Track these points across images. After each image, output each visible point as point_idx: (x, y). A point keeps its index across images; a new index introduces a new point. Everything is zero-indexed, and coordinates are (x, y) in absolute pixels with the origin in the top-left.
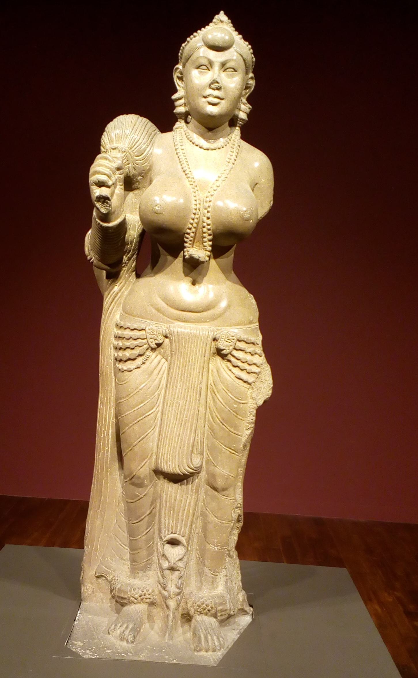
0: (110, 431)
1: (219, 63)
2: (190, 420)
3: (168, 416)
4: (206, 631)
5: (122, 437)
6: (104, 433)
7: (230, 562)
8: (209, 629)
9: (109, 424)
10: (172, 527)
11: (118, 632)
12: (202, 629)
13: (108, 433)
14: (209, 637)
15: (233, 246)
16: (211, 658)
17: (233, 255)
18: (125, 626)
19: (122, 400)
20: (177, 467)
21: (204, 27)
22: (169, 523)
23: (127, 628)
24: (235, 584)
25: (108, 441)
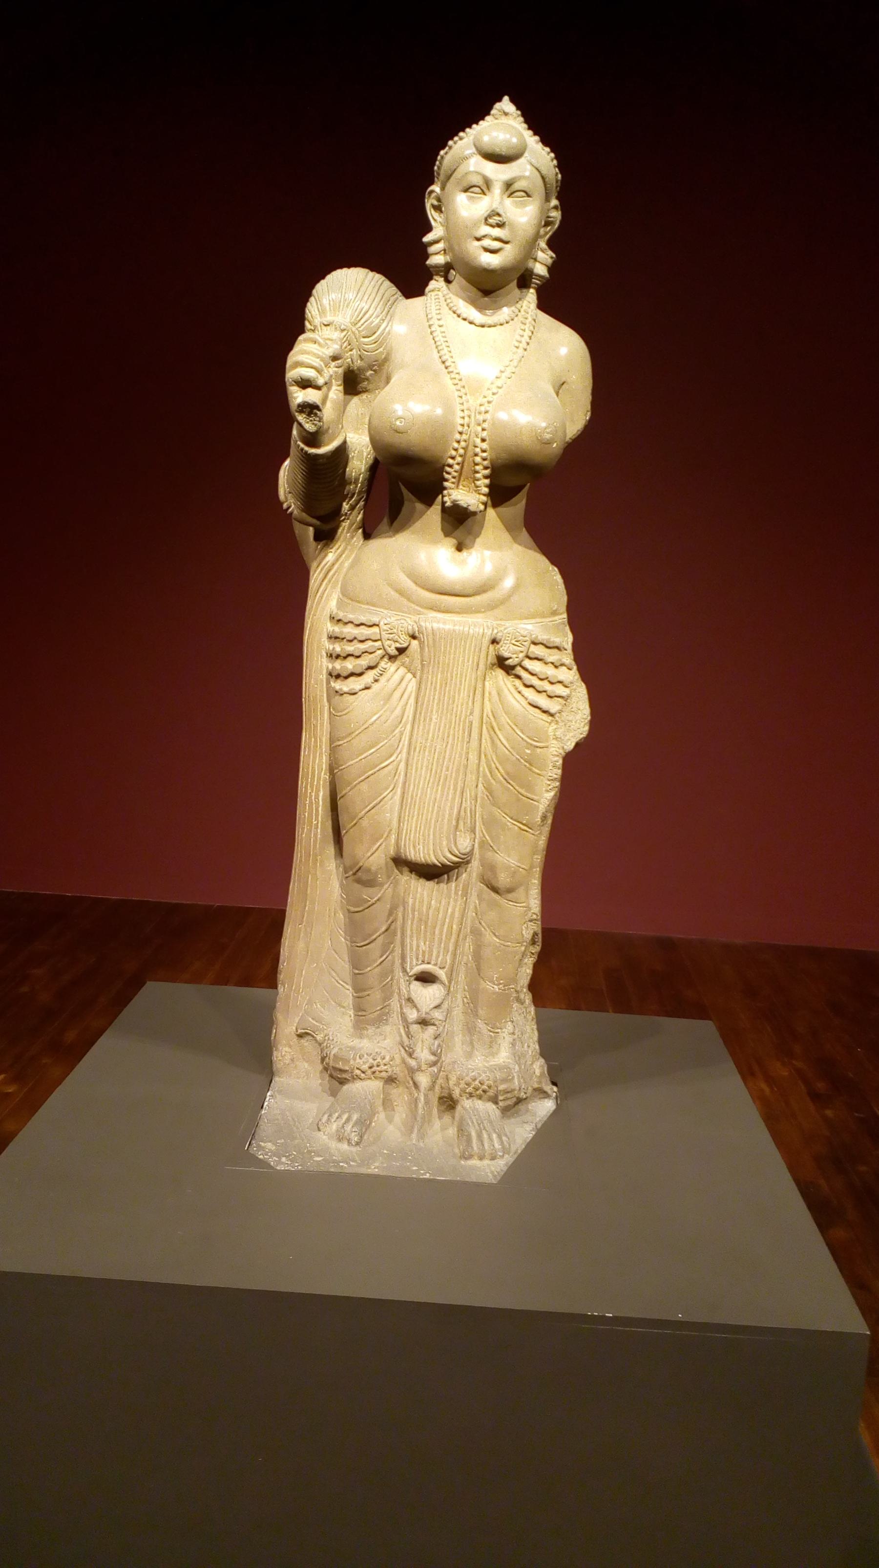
0: (321, 794)
4: (479, 1125)
6: (311, 796)
10: (424, 952)
11: (334, 1127)
12: (473, 1122)
13: (317, 797)
14: (485, 1136)
16: (488, 1170)
18: (345, 1117)
20: (431, 852)
22: (418, 946)
23: (348, 1120)
24: (529, 1047)
25: (317, 810)
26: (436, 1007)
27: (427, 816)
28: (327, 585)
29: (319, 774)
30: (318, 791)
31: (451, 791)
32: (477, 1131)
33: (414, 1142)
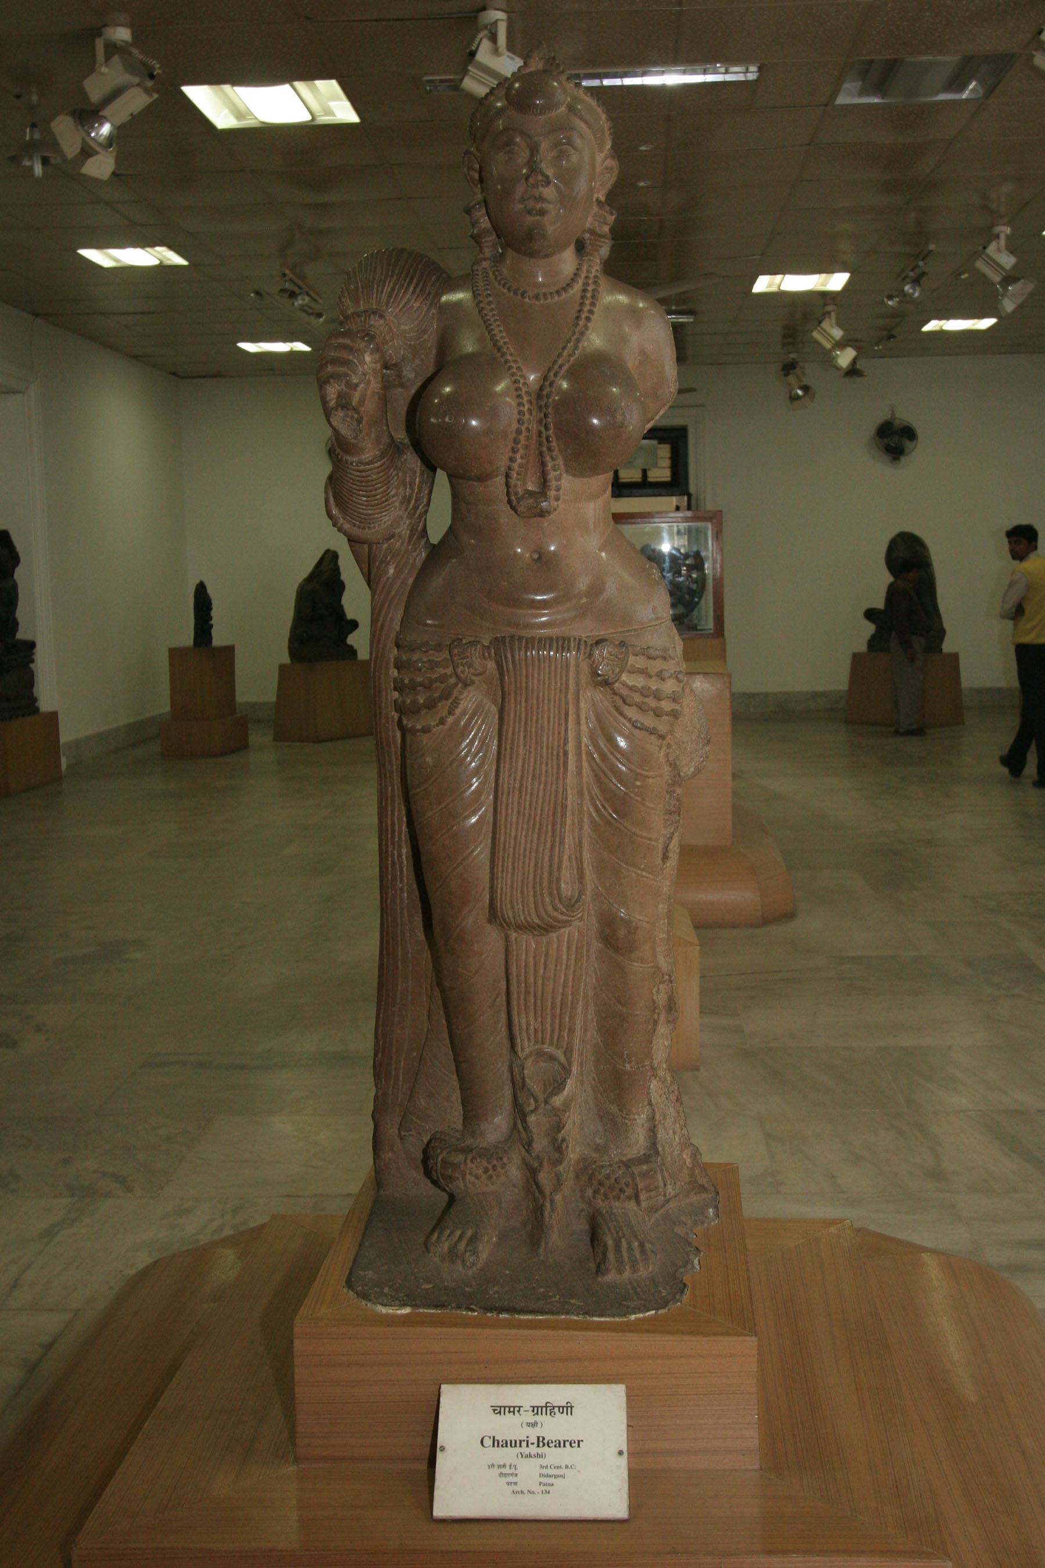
0: (404, 851)
1: (619, 526)
2: (551, 818)
3: (507, 814)
4: (617, 1233)
5: (423, 859)
6: (393, 855)
7: (660, 1092)
8: (625, 1229)
9: (400, 838)
10: (536, 1030)
11: (446, 1246)
12: (609, 1229)
13: (400, 855)
14: (624, 1242)
15: (599, 93)
16: (629, 1287)
17: (630, 365)
18: (458, 1233)
19: (418, 790)
20: (534, 915)
21: (211, 619)
22: (528, 1025)
23: (461, 1237)
24: (674, 1133)
25: (401, 871)
26: (1026, 204)
27: (523, 868)
28: (389, 607)
29: (400, 828)
30: (400, 847)
31: (549, 840)
32: (615, 1240)
33: (542, 1258)
